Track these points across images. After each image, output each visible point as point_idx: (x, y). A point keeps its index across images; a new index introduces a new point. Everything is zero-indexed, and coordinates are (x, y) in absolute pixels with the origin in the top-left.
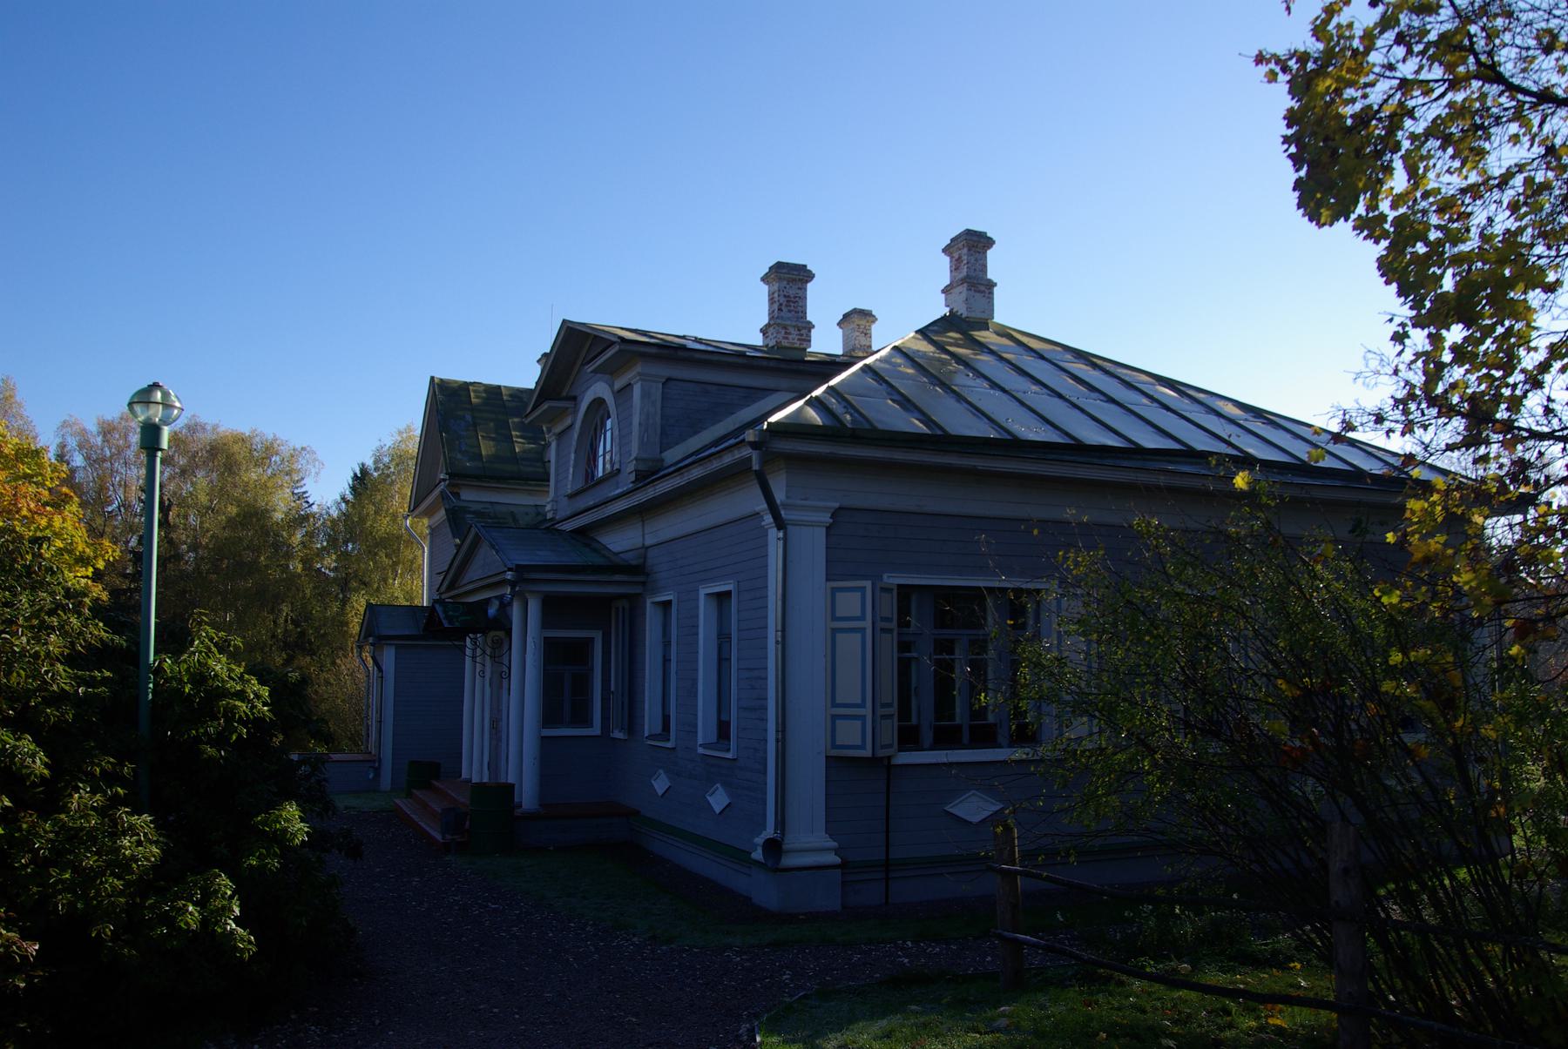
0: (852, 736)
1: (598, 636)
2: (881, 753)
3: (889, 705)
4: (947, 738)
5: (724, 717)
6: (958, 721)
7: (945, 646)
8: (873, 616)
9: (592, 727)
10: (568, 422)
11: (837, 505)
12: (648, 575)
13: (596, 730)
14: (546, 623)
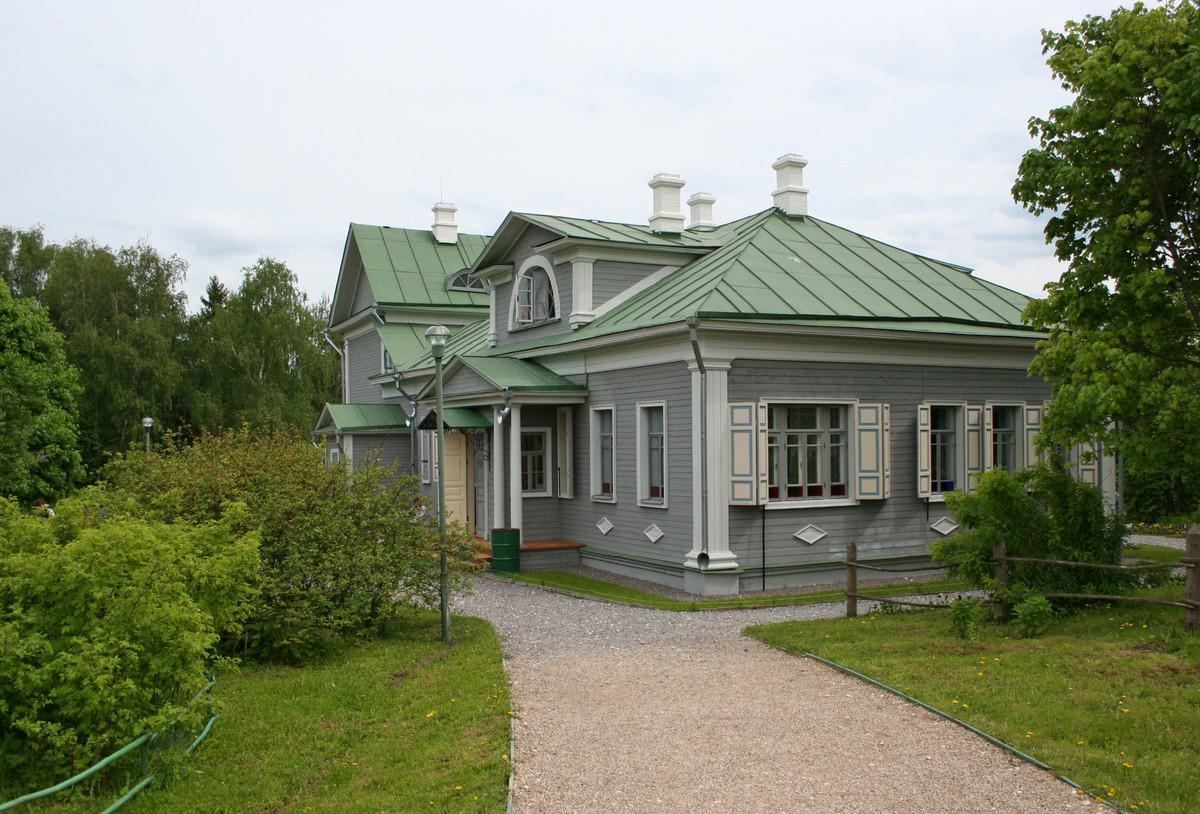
0: (744, 495)
1: (548, 431)
2: (761, 503)
3: (927, 470)
4: (795, 493)
5: (607, 481)
6: (800, 485)
7: (791, 439)
8: (757, 423)
9: (545, 491)
10: (509, 279)
11: (733, 357)
12: (590, 392)
13: (549, 493)
14: (523, 424)
